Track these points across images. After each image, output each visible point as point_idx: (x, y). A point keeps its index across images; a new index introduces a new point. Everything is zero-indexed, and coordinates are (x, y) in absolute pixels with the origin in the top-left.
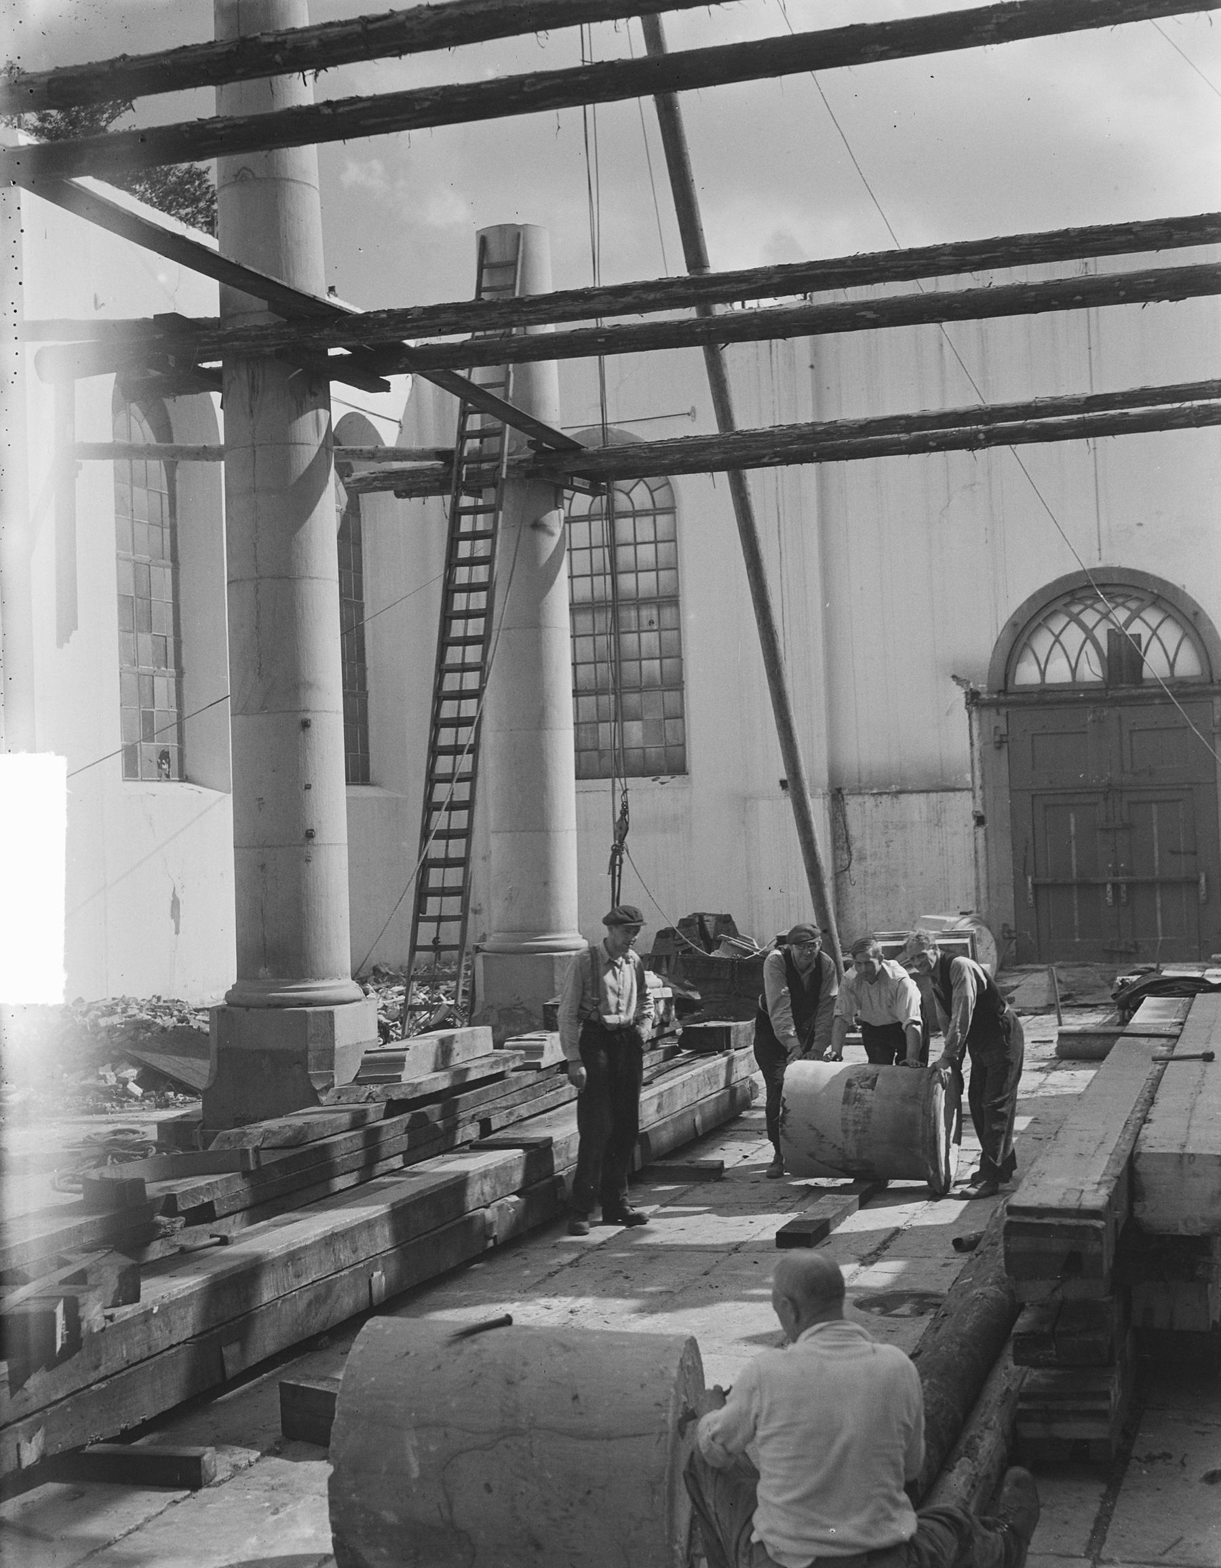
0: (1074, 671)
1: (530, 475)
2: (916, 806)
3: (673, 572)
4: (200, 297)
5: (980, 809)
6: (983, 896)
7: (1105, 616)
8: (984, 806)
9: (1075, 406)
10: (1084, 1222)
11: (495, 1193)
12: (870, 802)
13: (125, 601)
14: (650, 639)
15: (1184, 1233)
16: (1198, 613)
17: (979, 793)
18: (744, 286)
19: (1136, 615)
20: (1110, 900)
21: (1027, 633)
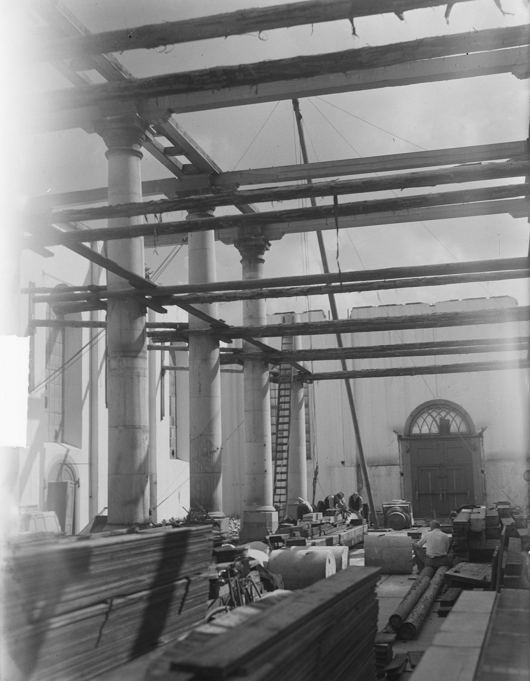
0: (430, 430)
1: (298, 380)
2: (383, 470)
4: (103, 278)
5: (402, 471)
7: (439, 414)
16: (466, 413)
17: (401, 466)
19: (448, 414)
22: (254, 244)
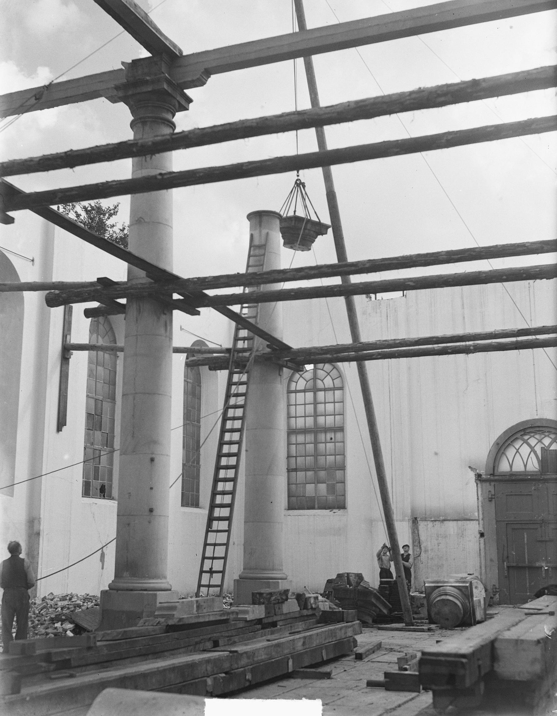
2: (452, 527)
3: (342, 416)
5: (481, 529)
6: (483, 571)
7: (540, 441)
8: (484, 528)
9: (513, 334)
10: (457, 659)
11: (213, 671)
12: (430, 524)
13: (89, 416)
14: (330, 446)
15: (519, 679)
17: (481, 522)
18: (353, 268)
20: (544, 575)
21: (504, 447)
22: (150, 89)
